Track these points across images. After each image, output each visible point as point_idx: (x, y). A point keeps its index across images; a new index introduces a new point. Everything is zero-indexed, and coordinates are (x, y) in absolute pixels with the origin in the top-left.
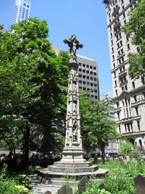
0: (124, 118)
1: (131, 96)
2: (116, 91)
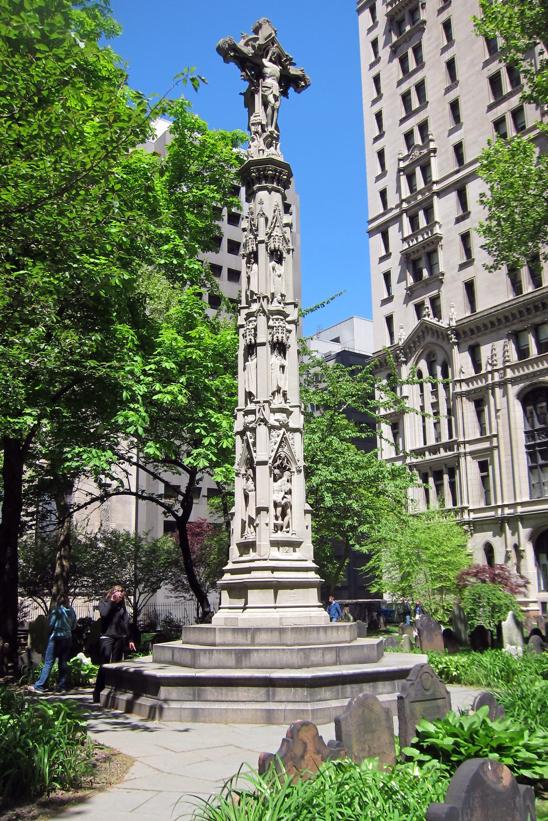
0: (420, 445)
1: (457, 344)
2: (389, 320)
